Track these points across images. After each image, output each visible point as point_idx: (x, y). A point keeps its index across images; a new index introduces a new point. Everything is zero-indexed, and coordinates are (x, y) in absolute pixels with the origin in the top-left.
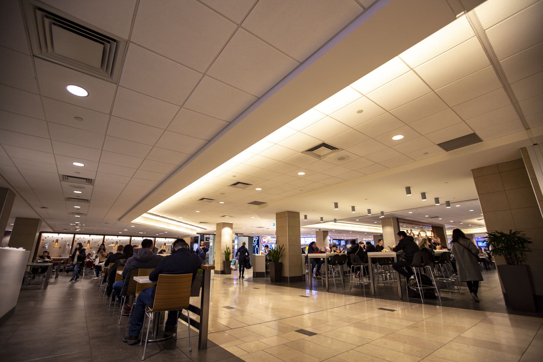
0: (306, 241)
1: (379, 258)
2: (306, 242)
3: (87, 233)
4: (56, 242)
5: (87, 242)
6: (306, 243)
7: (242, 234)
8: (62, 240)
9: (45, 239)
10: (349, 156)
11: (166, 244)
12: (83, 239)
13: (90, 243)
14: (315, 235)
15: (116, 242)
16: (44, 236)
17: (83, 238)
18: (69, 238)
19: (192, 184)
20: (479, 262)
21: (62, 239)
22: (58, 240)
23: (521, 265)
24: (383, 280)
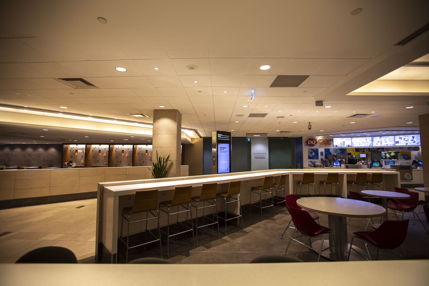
0: (396, 140)
1: (383, 190)
2: (398, 142)
3: (97, 143)
4: (76, 152)
5: (75, 152)
6: (397, 145)
7: (266, 134)
8: (129, 150)
9: (116, 150)
10: (75, 89)
11: (78, 151)
12: (120, 148)
13: (101, 152)
14: (418, 129)
15: (122, 150)
16: (116, 147)
17: (120, 147)
18: (102, 149)
19: (393, 71)
20: (398, 205)
21: (128, 149)
22: (123, 151)
23: (191, 209)
24: (100, 246)
